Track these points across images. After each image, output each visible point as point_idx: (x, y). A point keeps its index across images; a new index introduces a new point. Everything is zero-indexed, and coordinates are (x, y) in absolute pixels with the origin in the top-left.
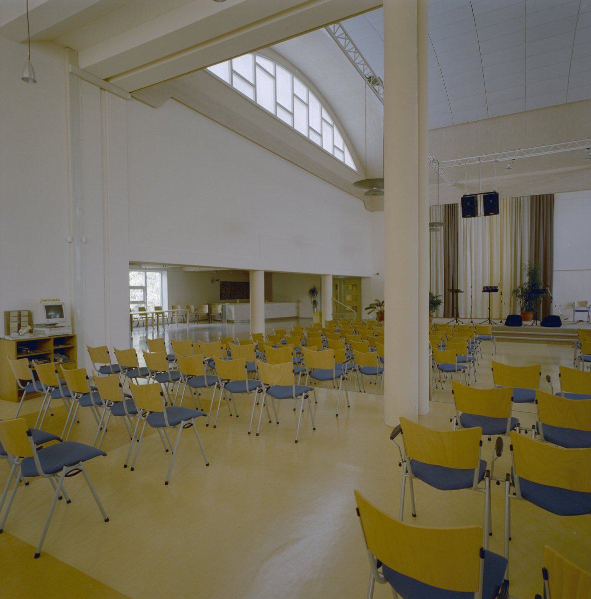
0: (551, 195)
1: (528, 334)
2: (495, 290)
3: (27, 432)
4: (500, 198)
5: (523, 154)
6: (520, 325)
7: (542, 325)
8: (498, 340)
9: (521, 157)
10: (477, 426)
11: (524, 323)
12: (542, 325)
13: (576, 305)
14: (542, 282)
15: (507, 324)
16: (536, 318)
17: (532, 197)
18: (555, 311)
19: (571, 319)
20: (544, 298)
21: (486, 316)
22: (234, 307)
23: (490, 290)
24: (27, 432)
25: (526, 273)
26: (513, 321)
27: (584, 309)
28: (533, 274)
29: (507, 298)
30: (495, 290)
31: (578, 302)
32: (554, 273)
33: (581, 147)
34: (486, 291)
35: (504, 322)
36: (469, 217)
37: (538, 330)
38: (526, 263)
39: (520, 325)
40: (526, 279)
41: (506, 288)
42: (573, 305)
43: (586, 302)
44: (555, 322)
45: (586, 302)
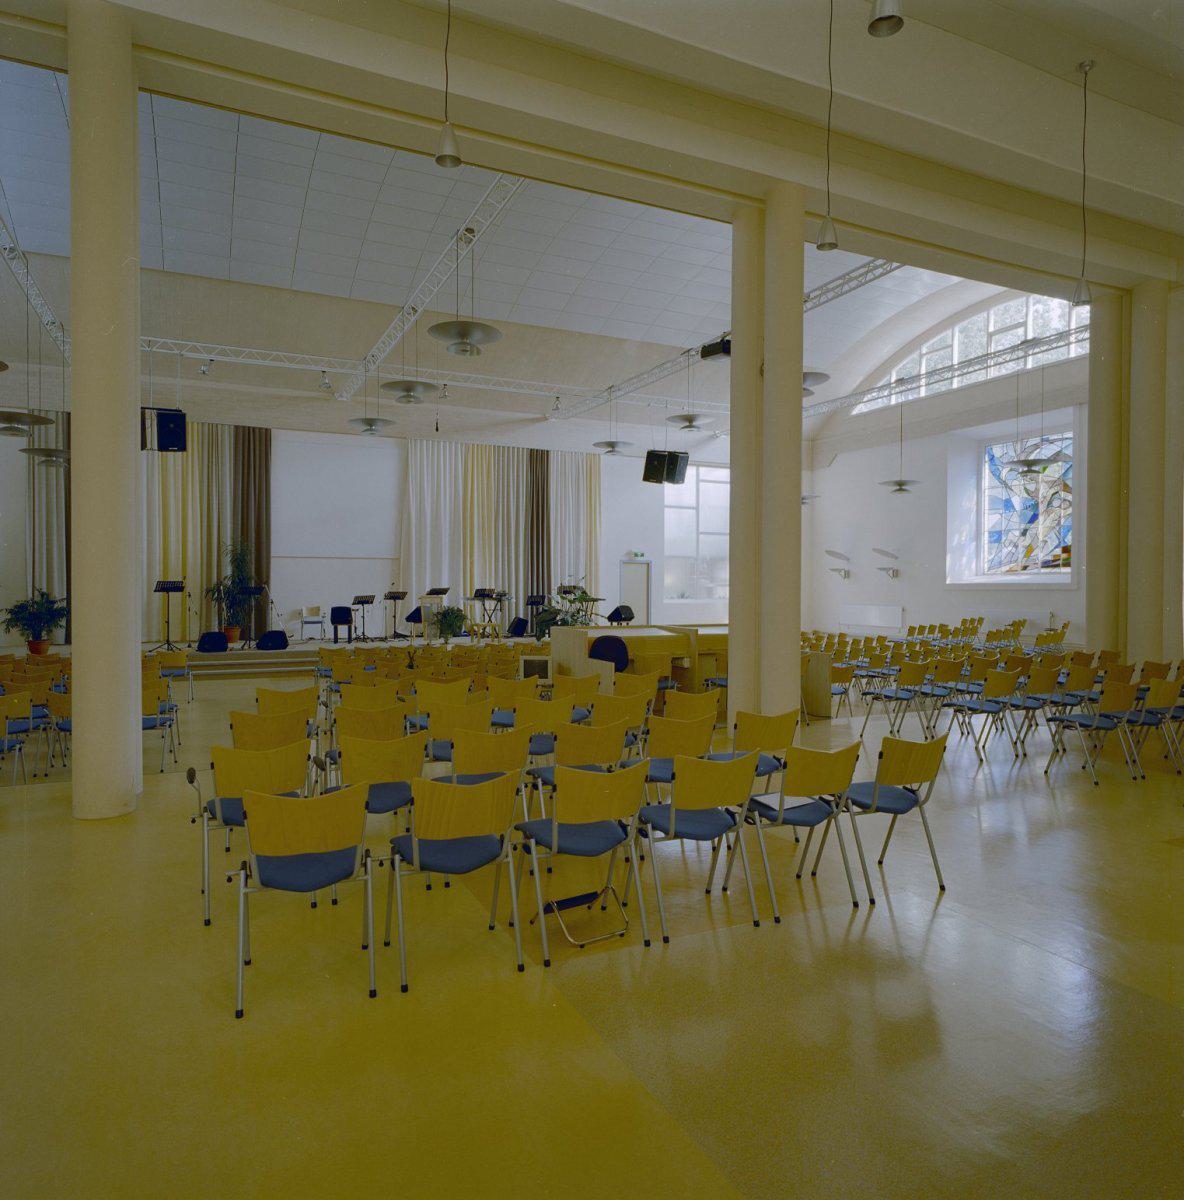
0: (266, 430)
1: (239, 664)
2: (178, 587)
3: (371, 991)
4: (187, 420)
5: (198, 351)
6: (224, 649)
7: (259, 647)
8: (196, 677)
9: (303, 367)
10: (835, 754)
11: (230, 645)
12: (259, 647)
13: (305, 614)
14: (253, 574)
15: (201, 648)
16: (244, 636)
17: (237, 427)
18: (276, 624)
19: (297, 637)
20: (256, 600)
21: (162, 638)
22: (965, 578)
23: (166, 587)
24: (371, 991)
25: (228, 558)
26: (212, 643)
27: (316, 619)
28: (239, 562)
29: (195, 604)
30: (178, 587)
31: (307, 608)
32: (273, 561)
33: (313, 367)
34: (159, 591)
35: (195, 646)
36: (174, 451)
37: (247, 656)
38: (229, 542)
39: (224, 649)
40: (228, 571)
41: (194, 584)
42: (300, 613)
43: (318, 609)
44: (278, 640)
45: (318, 609)
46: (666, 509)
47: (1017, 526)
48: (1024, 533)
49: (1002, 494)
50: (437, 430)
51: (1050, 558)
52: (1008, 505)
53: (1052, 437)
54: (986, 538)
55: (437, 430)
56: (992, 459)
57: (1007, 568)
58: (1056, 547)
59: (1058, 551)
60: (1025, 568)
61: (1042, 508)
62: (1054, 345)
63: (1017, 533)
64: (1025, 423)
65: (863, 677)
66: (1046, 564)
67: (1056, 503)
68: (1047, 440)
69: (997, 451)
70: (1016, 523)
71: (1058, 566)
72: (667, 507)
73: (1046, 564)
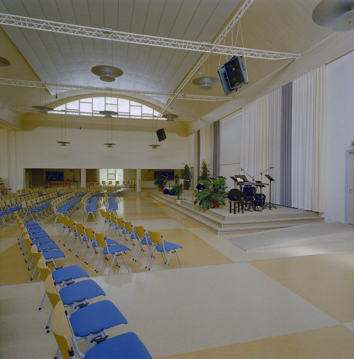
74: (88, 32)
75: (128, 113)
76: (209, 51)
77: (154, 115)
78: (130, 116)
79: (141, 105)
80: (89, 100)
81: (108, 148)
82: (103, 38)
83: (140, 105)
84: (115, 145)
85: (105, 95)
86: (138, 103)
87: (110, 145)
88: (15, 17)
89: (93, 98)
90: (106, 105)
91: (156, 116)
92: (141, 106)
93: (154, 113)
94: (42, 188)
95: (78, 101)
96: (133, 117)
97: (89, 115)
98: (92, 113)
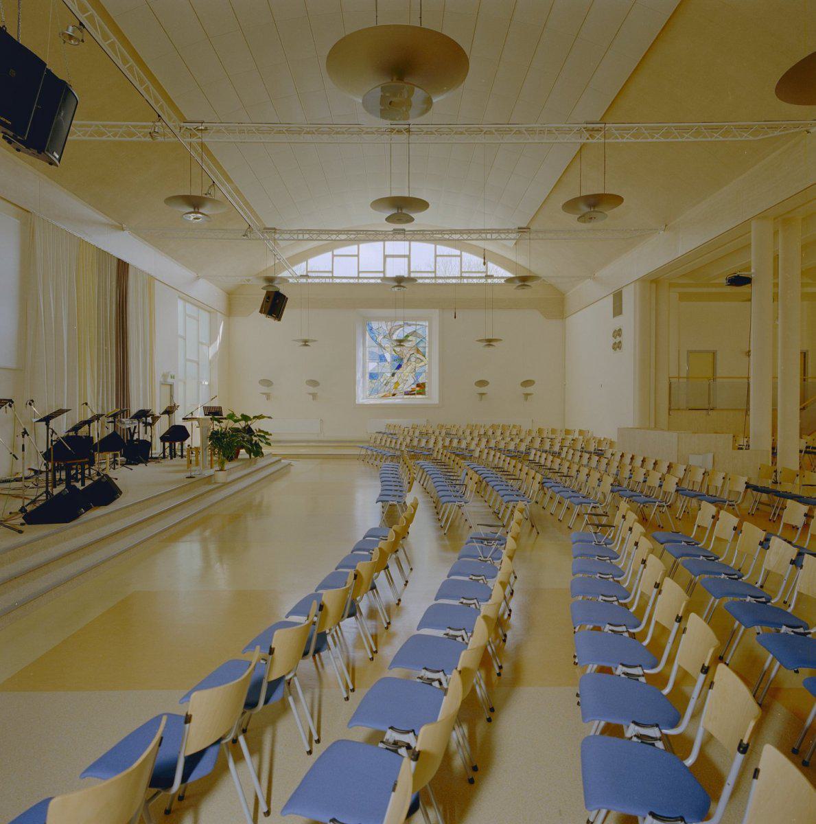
3: (620, 348)
46: (356, 246)
47: (389, 371)
48: (393, 375)
49: (376, 350)
50: (455, 317)
51: (409, 389)
52: (382, 358)
53: (409, 322)
54: (368, 376)
55: (455, 317)
56: (371, 329)
57: (383, 394)
58: (413, 384)
59: (414, 386)
60: (394, 395)
61: (405, 361)
62: (446, 236)
63: (389, 375)
64: (400, 312)
65: (90, 472)
66: (407, 393)
67: (413, 359)
68: (407, 324)
69: (375, 325)
70: (387, 369)
71: (414, 394)
72: (359, 246)
73: (407, 393)
74: (79, 136)
75: (433, 272)
76: (622, 139)
77: (489, 274)
78: (333, 277)
79: (459, 254)
80: (352, 249)
81: (487, 348)
82: (140, 139)
83: (457, 252)
84: (315, 343)
85: (435, 241)
86: (448, 249)
87: (489, 342)
88: (138, 126)
89: (438, 246)
90: (388, 260)
91: (491, 277)
92: (460, 256)
93: (334, 269)
94: (136, 437)
95: (330, 253)
96: (338, 281)
97: (352, 281)
98: (358, 278)
